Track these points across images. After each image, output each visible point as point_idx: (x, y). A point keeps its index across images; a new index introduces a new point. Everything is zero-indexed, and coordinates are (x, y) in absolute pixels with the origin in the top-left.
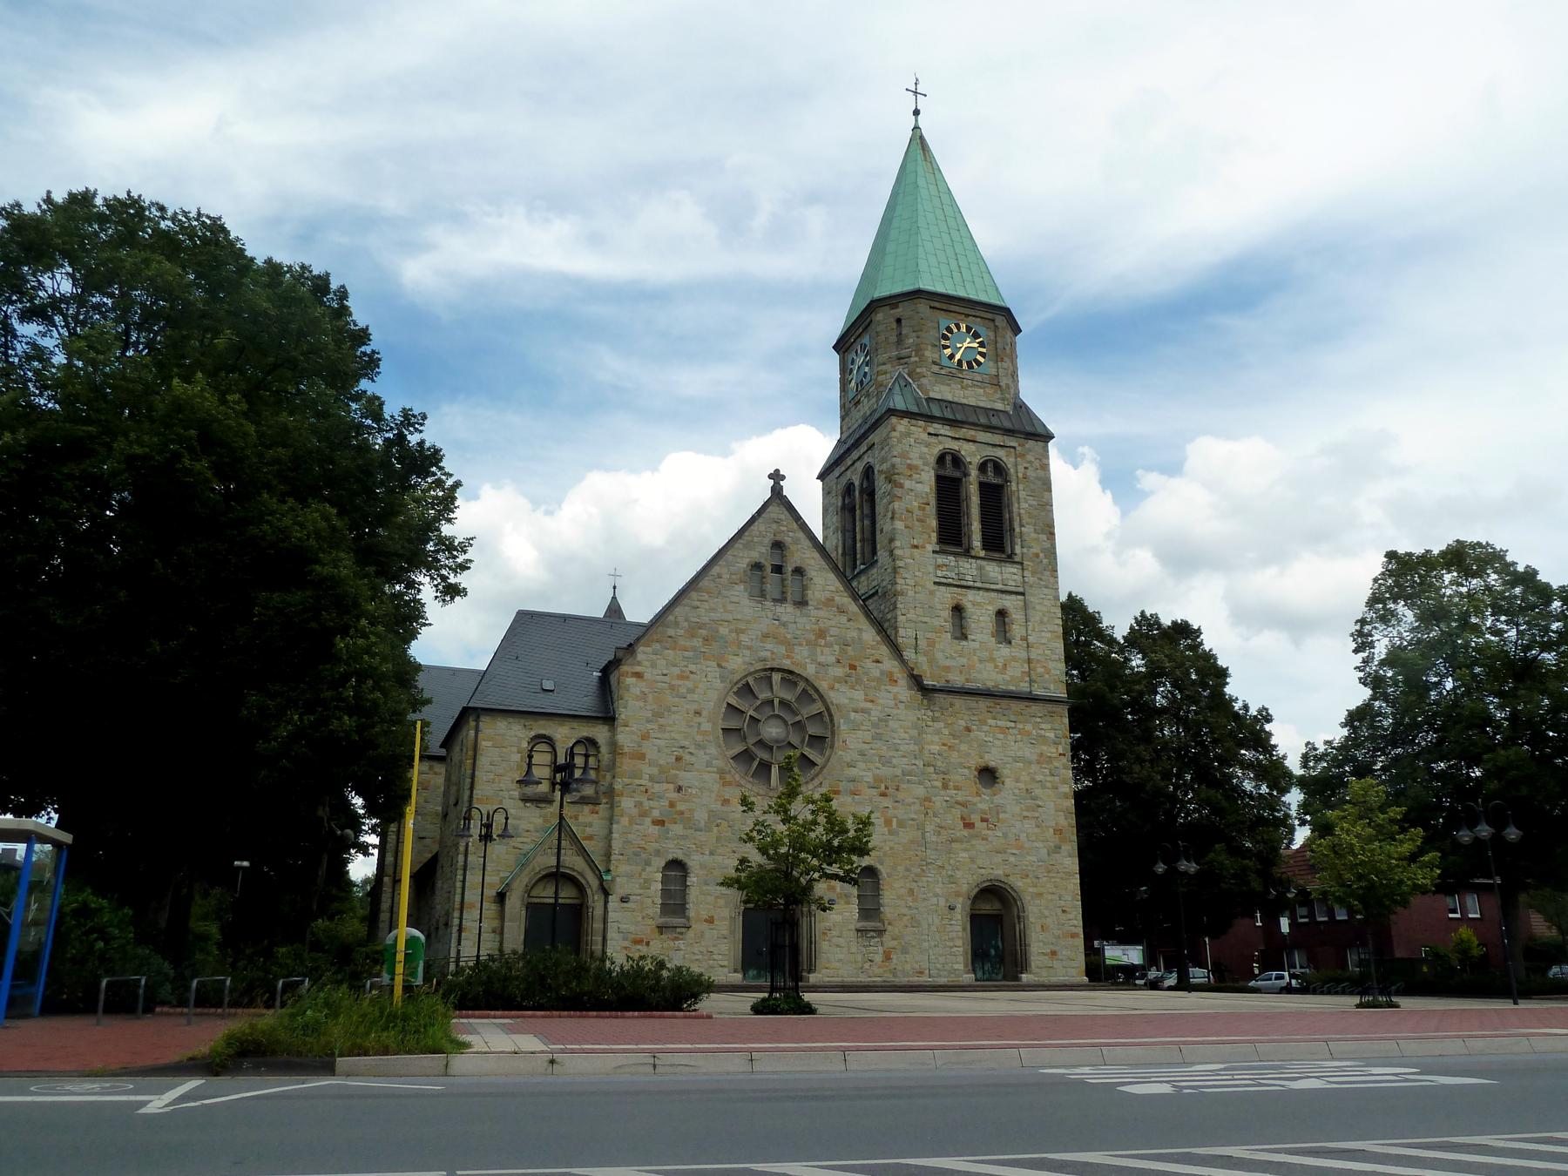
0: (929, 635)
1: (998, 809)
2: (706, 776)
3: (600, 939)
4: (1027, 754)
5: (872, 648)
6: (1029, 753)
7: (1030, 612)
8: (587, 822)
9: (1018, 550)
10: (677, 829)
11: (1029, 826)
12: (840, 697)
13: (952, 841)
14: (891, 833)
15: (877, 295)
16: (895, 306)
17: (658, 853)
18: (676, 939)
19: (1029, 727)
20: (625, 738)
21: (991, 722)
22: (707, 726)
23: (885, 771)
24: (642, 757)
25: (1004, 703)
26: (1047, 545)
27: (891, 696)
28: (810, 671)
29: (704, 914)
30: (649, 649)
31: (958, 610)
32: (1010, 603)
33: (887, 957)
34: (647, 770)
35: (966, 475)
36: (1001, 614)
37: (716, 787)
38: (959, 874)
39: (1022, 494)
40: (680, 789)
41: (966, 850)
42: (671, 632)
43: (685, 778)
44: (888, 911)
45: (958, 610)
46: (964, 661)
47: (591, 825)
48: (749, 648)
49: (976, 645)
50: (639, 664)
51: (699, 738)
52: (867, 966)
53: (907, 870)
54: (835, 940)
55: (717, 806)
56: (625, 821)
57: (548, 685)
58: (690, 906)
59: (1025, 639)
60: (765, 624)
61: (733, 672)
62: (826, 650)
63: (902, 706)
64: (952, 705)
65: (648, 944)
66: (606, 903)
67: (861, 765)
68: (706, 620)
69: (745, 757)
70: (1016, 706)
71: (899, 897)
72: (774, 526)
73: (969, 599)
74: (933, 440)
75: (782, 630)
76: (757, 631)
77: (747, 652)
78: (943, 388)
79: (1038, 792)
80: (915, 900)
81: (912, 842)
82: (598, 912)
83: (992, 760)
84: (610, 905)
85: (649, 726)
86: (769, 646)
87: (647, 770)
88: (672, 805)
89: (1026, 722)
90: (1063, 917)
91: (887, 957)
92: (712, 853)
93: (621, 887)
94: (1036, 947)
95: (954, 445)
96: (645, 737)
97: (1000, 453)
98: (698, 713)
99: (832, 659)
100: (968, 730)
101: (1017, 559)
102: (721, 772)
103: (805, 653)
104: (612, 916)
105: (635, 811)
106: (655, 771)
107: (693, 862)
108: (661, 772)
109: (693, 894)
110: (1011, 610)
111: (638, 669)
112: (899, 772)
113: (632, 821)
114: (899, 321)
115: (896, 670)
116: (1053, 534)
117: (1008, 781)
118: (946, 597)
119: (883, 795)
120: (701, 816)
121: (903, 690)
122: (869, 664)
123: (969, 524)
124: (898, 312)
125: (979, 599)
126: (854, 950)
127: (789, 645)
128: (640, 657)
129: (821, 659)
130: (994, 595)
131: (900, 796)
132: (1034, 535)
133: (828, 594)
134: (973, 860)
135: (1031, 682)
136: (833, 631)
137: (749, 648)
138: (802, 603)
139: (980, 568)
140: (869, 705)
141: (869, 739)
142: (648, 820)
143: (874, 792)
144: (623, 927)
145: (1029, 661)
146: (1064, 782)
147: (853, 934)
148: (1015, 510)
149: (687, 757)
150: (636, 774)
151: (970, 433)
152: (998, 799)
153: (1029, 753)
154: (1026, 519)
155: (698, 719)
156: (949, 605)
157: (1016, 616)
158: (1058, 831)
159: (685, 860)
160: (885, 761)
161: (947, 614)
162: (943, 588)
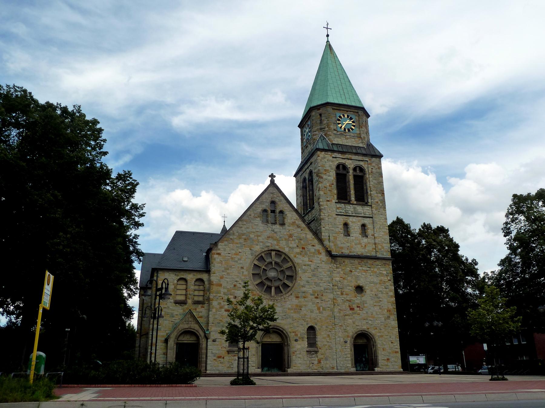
0: (334, 235)
1: (364, 302)
3: (205, 356)
4: (375, 280)
5: (311, 240)
6: (376, 280)
7: (375, 225)
9: (370, 200)
16: (319, 109)
19: (375, 270)
21: (360, 268)
22: (246, 273)
23: (317, 289)
24: (220, 285)
25: (365, 260)
28: (286, 250)
31: (346, 225)
32: (367, 221)
33: (319, 362)
35: (348, 172)
36: (363, 226)
38: (348, 328)
41: (351, 319)
42: (231, 237)
44: (319, 344)
45: (346, 225)
50: (219, 250)
52: (311, 365)
53: (327, 327)
56: (214, 310)
57: (185, 259)
59: (373, 235)
60: (268, 233)
62: (293, 242)
65: (223, 358)
66: (207, 342)
71: (324, 338)
72: (271, 195)
73: (350, 220)
74: (335, 159)
78: (339, 139)
79: (380, 295)
80: (330, 339)
81: (328, 316)
82: (204, 346)
84: (209, 343)
85: (223, 273)
91: (319, 362)
95: (343, 161)
96: (222, 278)
98: (242, 268)
106: (226, 291)
111: (219, 252)
112: (322, 289)
114: (320, 115)
116: (384, 194)
119: (316, 298)
121: (324, 257)
122: (310, 247)
125: (354, 220)
126: (306, 359)
129: (291, 245)
131: (323, 298)
132: (376, 195)
133: (293, 220)
135: (376, 252)
136: (296, 235)
137: (262, 242)
139: (354, 208)
140: (310, 263)
142: (223, 310)
143: (313, 297)
144: (213, 351)
146: (391, 291)
147: (305, 353)
148: (368, 185)
150: (218, 292)
153: (376, 280)
155: (242, 270)
157: (369, 226)
158: (389, 311)
160: (317, 285)
161: (341, 226)
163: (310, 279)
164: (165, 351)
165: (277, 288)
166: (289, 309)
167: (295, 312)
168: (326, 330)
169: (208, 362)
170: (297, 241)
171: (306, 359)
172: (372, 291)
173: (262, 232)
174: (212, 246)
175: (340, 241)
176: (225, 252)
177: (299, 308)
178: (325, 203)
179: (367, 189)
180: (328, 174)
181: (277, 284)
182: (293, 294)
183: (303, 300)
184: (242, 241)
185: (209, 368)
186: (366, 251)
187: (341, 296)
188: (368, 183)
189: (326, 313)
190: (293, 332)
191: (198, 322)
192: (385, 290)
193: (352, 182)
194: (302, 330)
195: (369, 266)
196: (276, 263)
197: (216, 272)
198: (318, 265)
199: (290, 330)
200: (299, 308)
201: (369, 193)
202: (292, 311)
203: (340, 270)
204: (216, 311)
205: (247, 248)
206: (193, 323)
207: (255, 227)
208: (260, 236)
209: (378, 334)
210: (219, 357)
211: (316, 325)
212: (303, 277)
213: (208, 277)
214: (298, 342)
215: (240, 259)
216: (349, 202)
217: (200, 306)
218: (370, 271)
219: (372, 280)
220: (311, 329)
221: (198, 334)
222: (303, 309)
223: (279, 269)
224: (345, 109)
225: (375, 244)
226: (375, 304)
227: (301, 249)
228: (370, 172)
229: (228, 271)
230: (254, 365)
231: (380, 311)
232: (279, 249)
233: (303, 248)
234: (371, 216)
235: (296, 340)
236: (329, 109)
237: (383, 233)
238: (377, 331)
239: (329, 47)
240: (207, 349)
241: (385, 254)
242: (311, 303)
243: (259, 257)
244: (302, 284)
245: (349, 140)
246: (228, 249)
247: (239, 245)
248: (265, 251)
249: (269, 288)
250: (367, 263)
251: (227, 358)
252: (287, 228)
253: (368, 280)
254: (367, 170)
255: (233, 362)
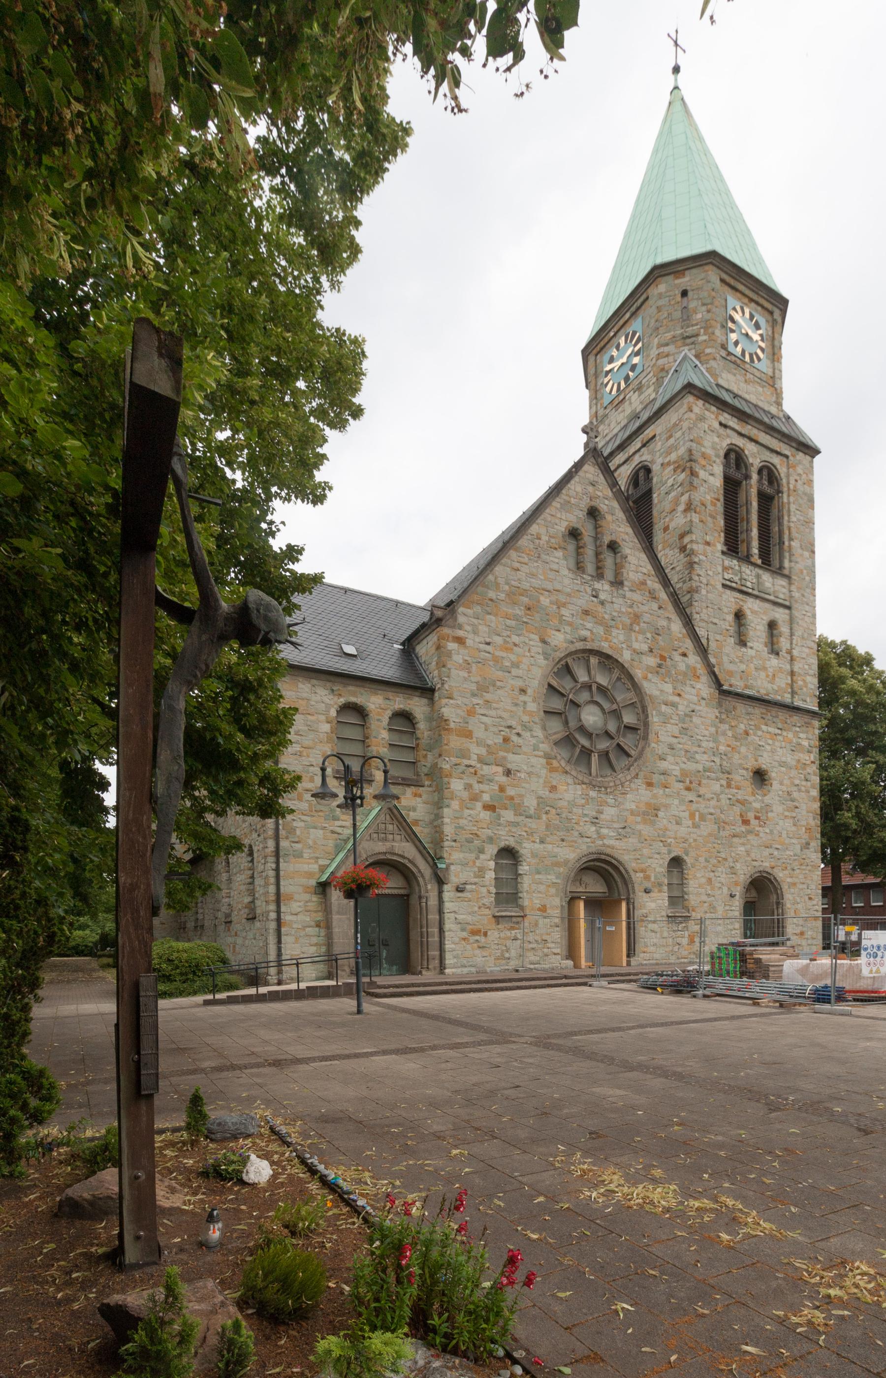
0: (718, 637)
1: (768, 807)
2: (534, 760)
3: (436, 930)
4: (789, 760)
5: (679, 640)
6: (790, 759)
7: (795, 626)
8: (414, 804)
9: (786, 564)
10: (508, 815)
11: (788, 824)
12: (653, 687)
13: (734, 836)
14: (696, 826)
15: (659, 260)
16: (679, 274)
17: (491, 840)
18: (512, 928)
19: (790, 735)
20: (450, 711)
21: (764, 727)
22: (532, 707)
23: (691, 766)
24: (469, 735)
25: (774, 711)
26: (809, 562)
27: (694, 691)
28: (625, 657)
29: (537, 903)
30: (469, 612)
31: (739, 616)
32: (780, 615)
34: (476, 750)
35: (747, 477)
36: (772, 625)
37: (544, 772)
38: (738, 866)
39: (793, 507)
40: (508, 773)
41: (743, 844)
42: (492, 594)
43: (514, 760)
44: (693, 900)
45: (739, 616)
46: (743, 667)
47: (414, 809)
48: (570, 624)
49: (751, 652)
50: (460, 627)
51: (526, 718)
52: (676, 948)
53: (707, 861)
54: (651, 926)
55: (545, 793)
56: (455, 804)
57: (350, 649)
58: (524, 895)
59: (789, 652)
60: (584, 601)
61: (556, 649)
62: (640, 637)
63: (703, 702)
64: (734, 708)
65: (485, 934)
66: (440, 892)
67: (670, 758)
68: (526, 585)
69: (568, 741)
70: (782, 715)
71: (700, 886)
72: (590, 489)
73: (751, 606)
74: (722, 430)
75: (600, 609)
76: (574, 608)
77: (568, 629)
78: (731, 377)
79: (795, 795)
80: (712, 889)
81: (710, 835)
82: (433, 902)
83: (765, 762)
84: (446, 896)
85: (475, 700)
86: (589, 625)
87: (476, 750)
88: (502, 789)
89: (789, 730)
90: (810, 903)
92: (542, 842)
93: (456, 875)
94: (791, 928)
95: (740, 442)
96: (471, 713)
97: (776, 460)
98: (523, 691)
99: (645, 647)
100: (747, 733)
101: (786, 572)
102: (548, 757)
103: (621, 638)
104: (448, 906)
105: (465, 795)
106: (483, 751)
107: (526, 849)
108: (490, 753)
109: (526, 883)
110: (780, 623)
111: (460, 633)
112: (700, 768)
113: (463, 806)
114: (684, 293)
115: (699, 666)
116: (813, 552)
117: (775, 783)
118: (730, 600)
119: (688, 789)
120: (531, 803)
121: (704, 687)
122: (677, 657)
123: (748, 531)
124: (684, 281)
125: (756, 608)
126: (665, 934)
127: (608, 628)
128: (461, 619)
129: (636, 645)
130: (767, 605)
131: (702, 791)
132: (800, 551)
133: (641, 577)
134: (748, 853)
135: (793, 693)
136: (646, 617)
137: (570, 624)
138: (618, 583)
139: (758, 576)
140: (676, 699)
141: (677, 734)
142: (479, 805)
143: (681, 786)
144: (460, 917)
145: (792, 673)
146: (813, 787)
148: (785, 522)
149: (515, 738)
150: (464, 754)
151: (754, 432)
152: (767, 799)
153: (790, 759)
154: (794, 534)
155: (523, 698)
156: (734, 608)
157: (784, 629)
158: (808, 830)
159: (518, 848)
160: (690, 756)
161: (730, 618)
162: (728, 592)
163: (675, 740)
164: (319, 916)
165: (605, 756)
166: (632, 813)
167: (645, 822)
168: (705, 867)
169: (448, 946)
170: (649, 635)
171: (665, 934)
172: (781, 784)
173: (569, 595)
174: (439, 613)
175: (728, 655)
176: (477, 639)
177: (652, 812)
178: (701, 547)
179: (781, 533)
180: (708, 467)
181: (603, 745)
182: (641, 774)
183: (661, 792)
184: (519, 611)
185: (449, 960)
186: (776, 688)
187: (727, 791)
188: (786, 518)
189: (708, 828)
190: (642, 871)
191: (413, 837)
192: (804, 783)
193: (755, 504)
194: (658, 866)
195: (780, 726)
196: (602, 690)
197: (455, 696)
198: (693, 706)
199: (634, 865)
200: (652, 812)
201: (787, 543)
202: (639, 819)
203: (727, 726)
204: (461, 808)
205: (533, 636)
206: (398, 837)
207: (552, 575)
208: (564, 605)
209: (789, 880)
210: (474, 933)
211: (687, 855)
212: (663, 732)
213: (427, 709)
214: (652, 894)
215: (516, 665)
216: (746, 559)
217: (409, 791)
218: (780, 738)
219: (784, 759)
220: (676, 863)
221: (414, 870)
222: (661, 814)
223: (606, 706)
224: (747, 292)
225: (792, 673)
226: (787, 813)
227: (658, 660)
228: (791, 487)
229: (488, 696)
230: (558, 951)
231: (794, 829)
232: (610, 652)
233: (663, 658)
234: (787, 603)
235: (647, 891)
236: (713, 275)
237: (807, 650)
238: (786, 872)
239: (677, 99)
240: (441, 912)
241: (808, 700)
242: (676, 802)
243: (559, 666)
244: (660, 752)
245: (750, 388)
246: (483, 629)
247: (513, 623)
248: (576, 652)
249: (586, 753)
250: (777, 717)
251: (493, 935)
252: (629, 594)
253: (777, 758)
254: (784, 481)
255: (509, 943)
